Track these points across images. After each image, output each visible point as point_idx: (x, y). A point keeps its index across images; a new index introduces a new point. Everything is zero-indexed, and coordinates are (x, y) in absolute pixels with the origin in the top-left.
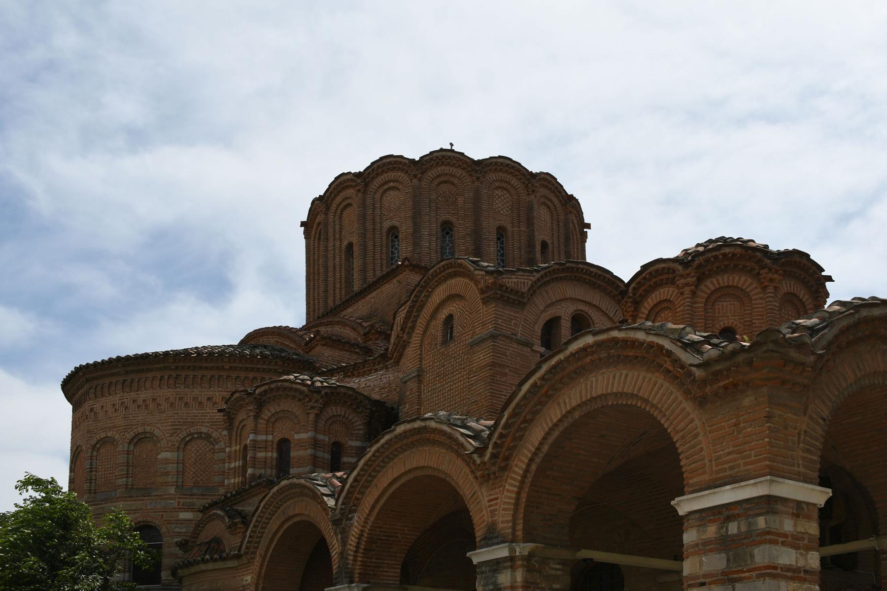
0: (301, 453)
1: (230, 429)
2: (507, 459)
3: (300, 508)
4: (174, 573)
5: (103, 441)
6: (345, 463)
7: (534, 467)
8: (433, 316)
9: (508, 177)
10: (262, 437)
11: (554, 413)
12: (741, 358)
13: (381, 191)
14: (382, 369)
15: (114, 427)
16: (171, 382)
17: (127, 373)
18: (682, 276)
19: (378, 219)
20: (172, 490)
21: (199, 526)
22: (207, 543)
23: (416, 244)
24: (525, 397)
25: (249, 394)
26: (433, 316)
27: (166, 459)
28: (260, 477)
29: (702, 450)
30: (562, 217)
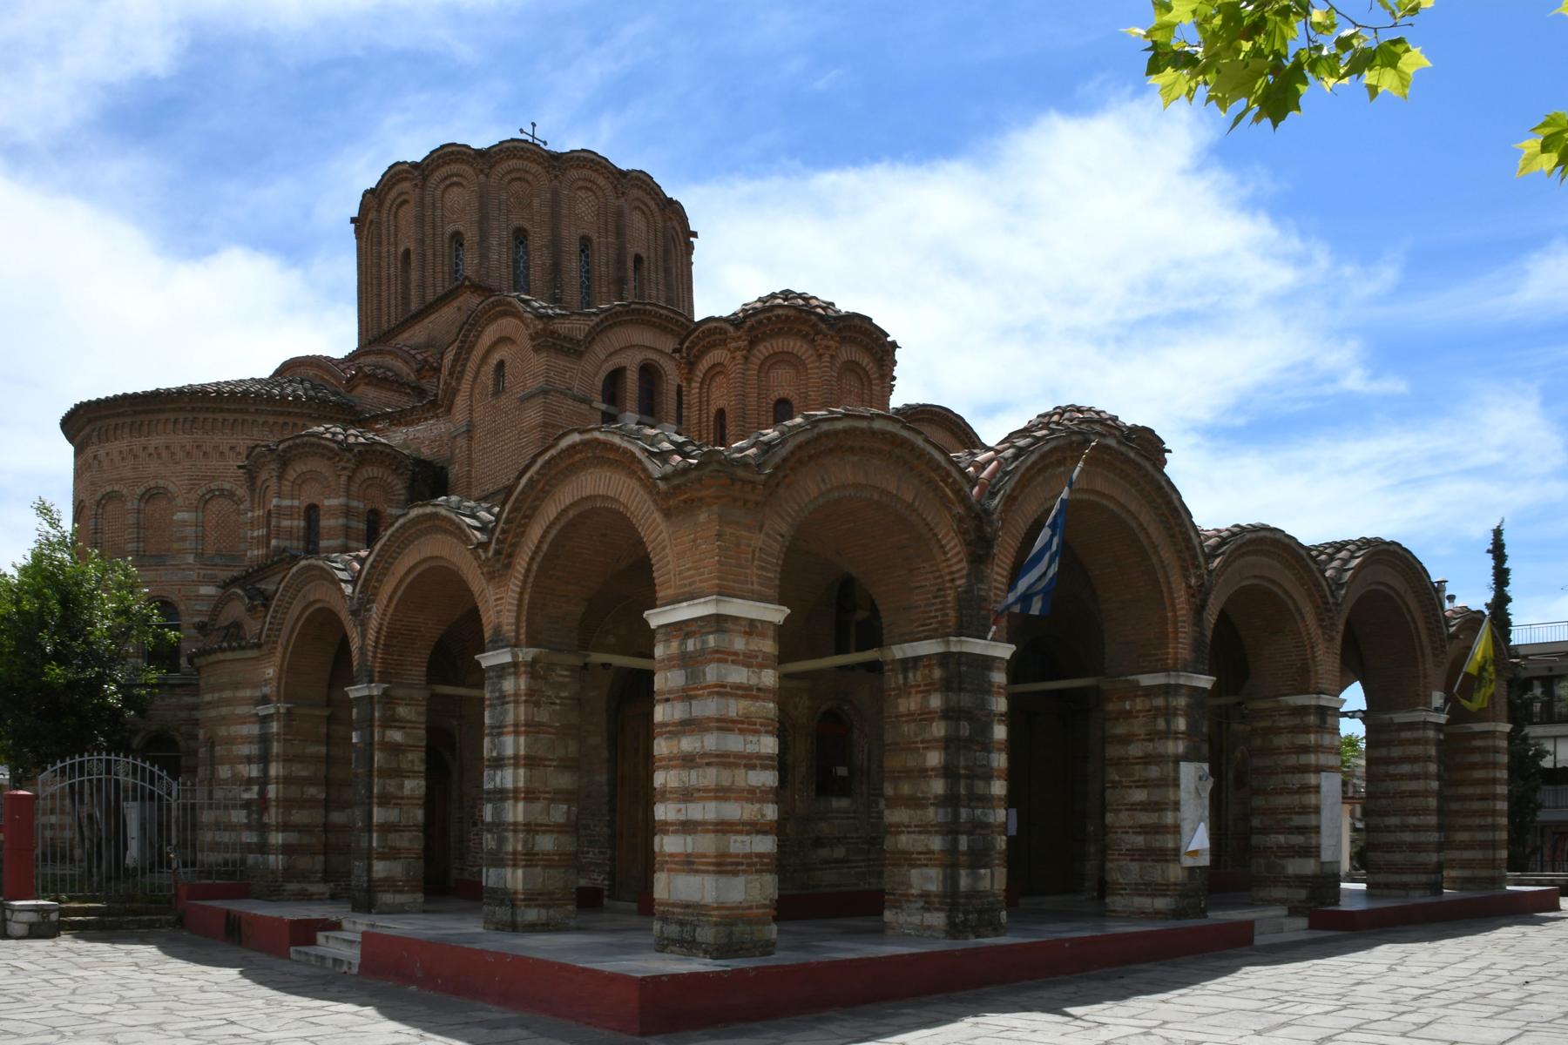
0: (332, 522)
2: (510, 555)
3: (318, 593)
4: (190, 661)
5: (109, 497)
7: (535, 567)
8: (484, 359)
10: (286, 502)
11: (550, 511)
12: (693, 475)
13: (442, 186)
16: (187, 426)
17: (135, 413)
19: (439, 223)
20: (191, 559)
21: (220, 604)
23: (483, 257)
24: (522, 492)
25: (271, 451)
26: (484, 359)
27: (184, 521)
28: (284, 550)
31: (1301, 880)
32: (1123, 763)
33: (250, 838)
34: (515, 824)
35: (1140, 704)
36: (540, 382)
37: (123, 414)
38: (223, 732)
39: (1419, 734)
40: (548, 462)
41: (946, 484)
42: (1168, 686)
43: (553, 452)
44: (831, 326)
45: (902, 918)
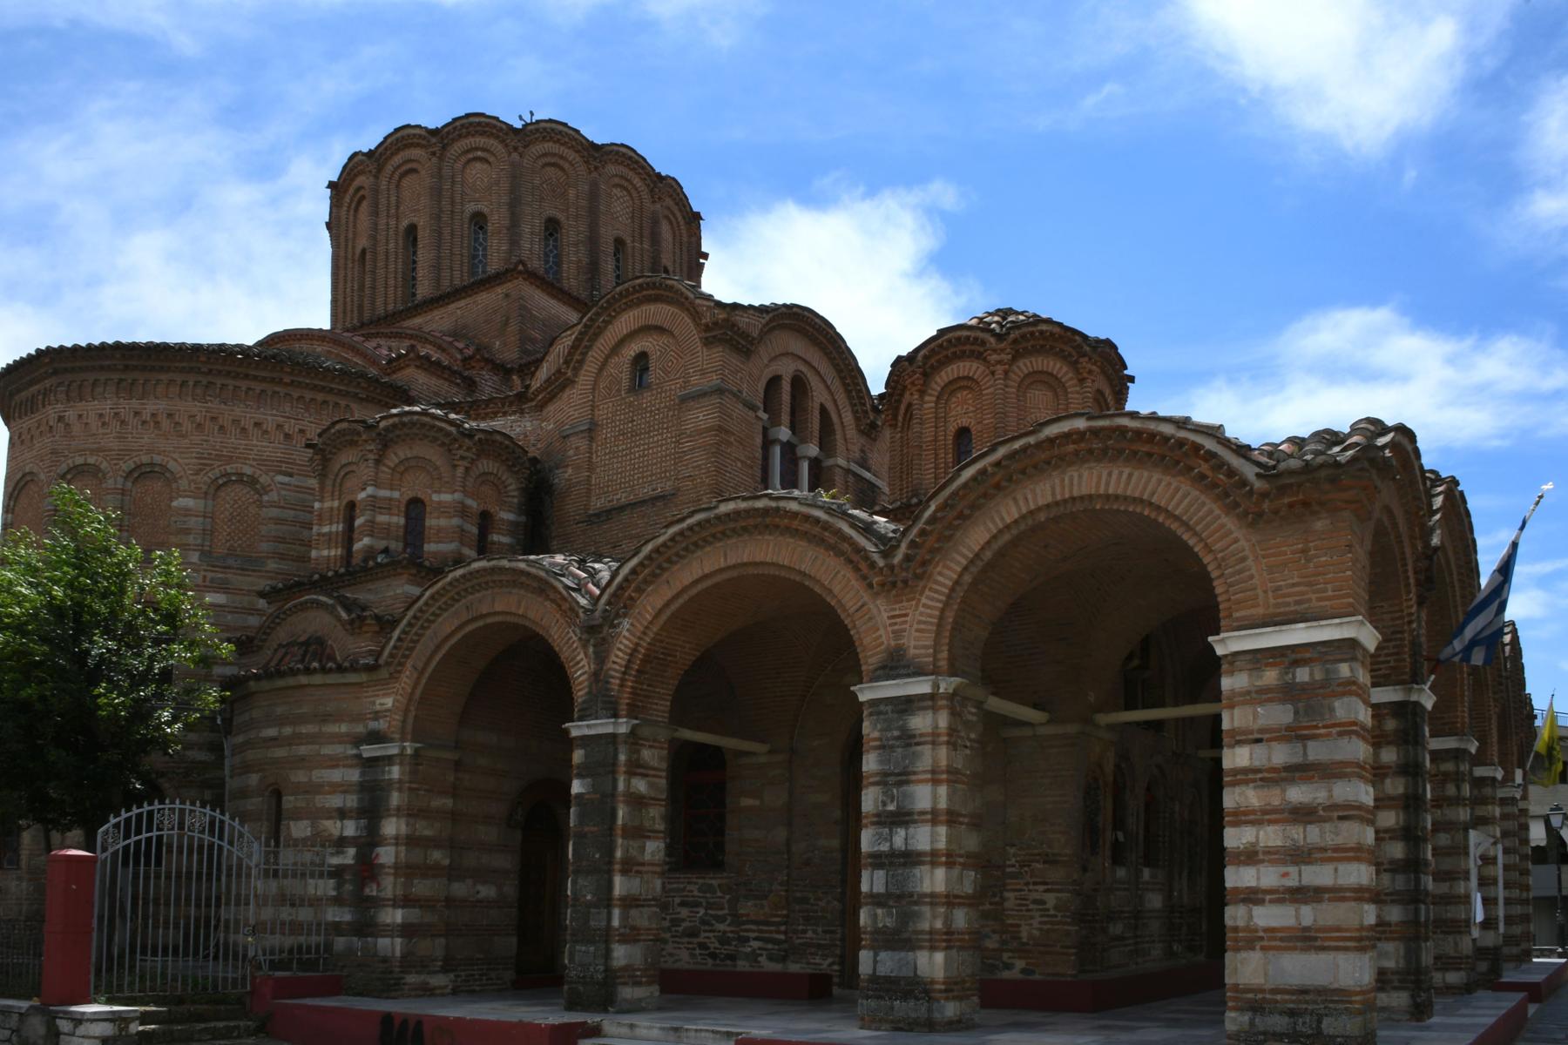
0: (443, 522)
1: (322, 476)
2: (924, 563)
6: (493, 543)
9: (631, 174)
11: (1007, 511)
12: (1323, 473)
13: (464, 159)
14: (514, 413)
15: (99, 450)
16: (199, 391)
17: (127, 367)
18: (995, 351)
22: (302, 644)
23: (514, 242)
24: (965, 485)
29: (1251, 577)
30: (685, 239)
33: (345, 916)
34: (933, 895)
36: (715, 380)
38: (300, 777)
42: (1457, 750)
43: (1031, 440)
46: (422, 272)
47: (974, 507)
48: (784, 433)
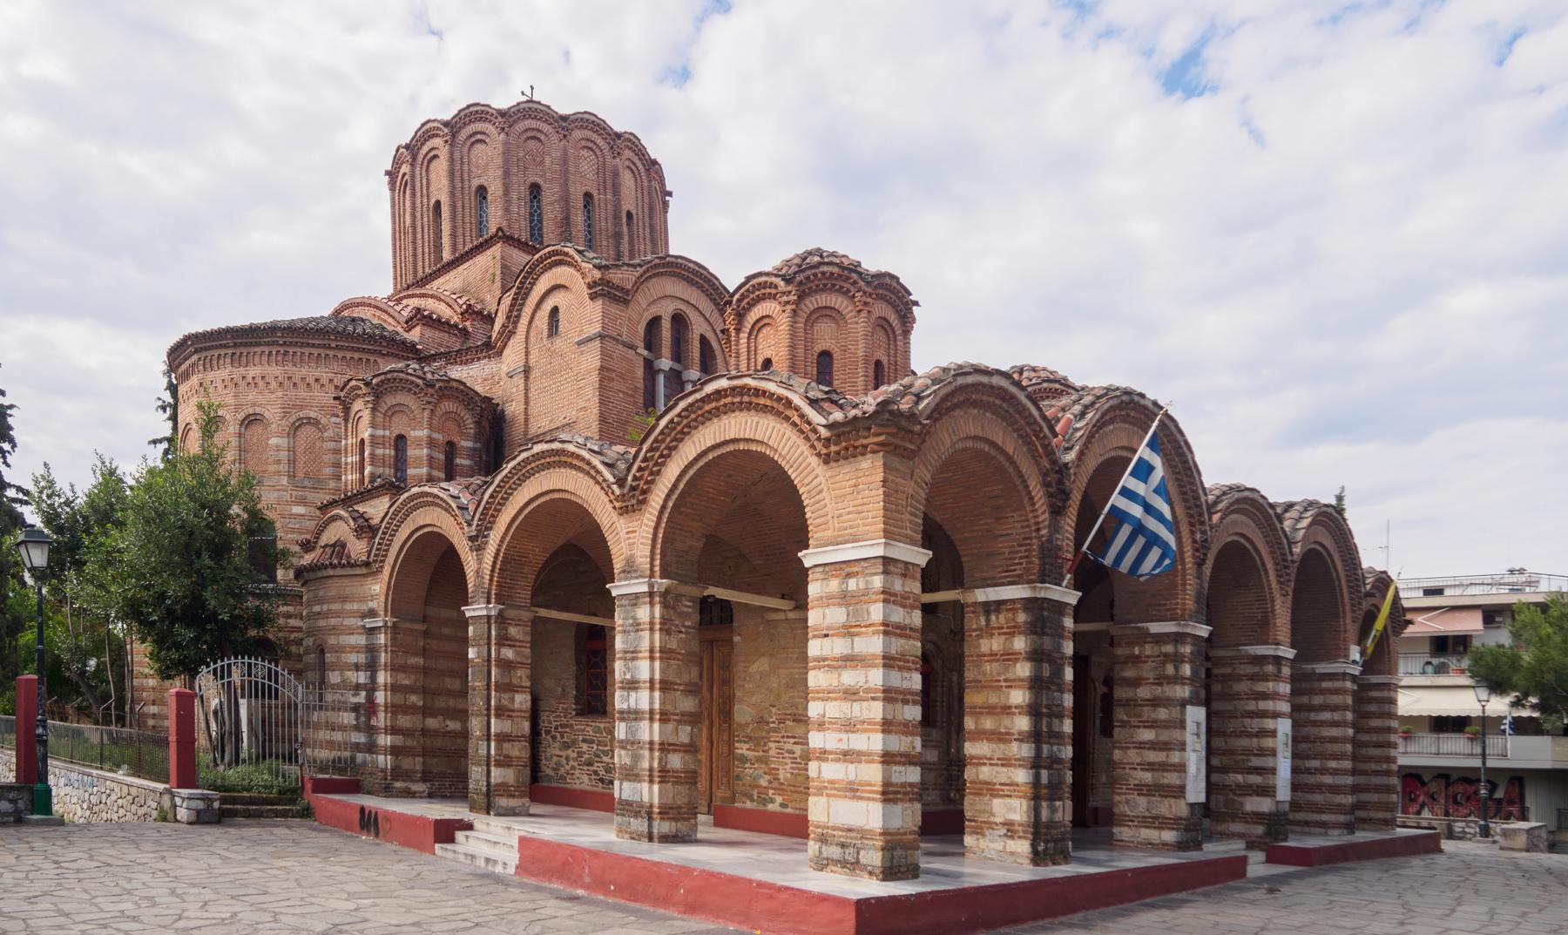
2: (644, 492)
7: (670, 504)
9: (594, 136)
10: (380, 432)
11: (689, 450)
17: (235, 345)
24: (662, 432)
31: (1258, 817)
32: (1129, 703)
33: (360, 738)
35: (1149, 650)
37: (226, 346)
39: (1338, 684)
40: (691, 405)
41: (1037, 437)
42: (1177, 634)
44: (868, 283)
45: (983, 843)
46: (446, 240)
47: (671, 449)
48: (665, 363)
